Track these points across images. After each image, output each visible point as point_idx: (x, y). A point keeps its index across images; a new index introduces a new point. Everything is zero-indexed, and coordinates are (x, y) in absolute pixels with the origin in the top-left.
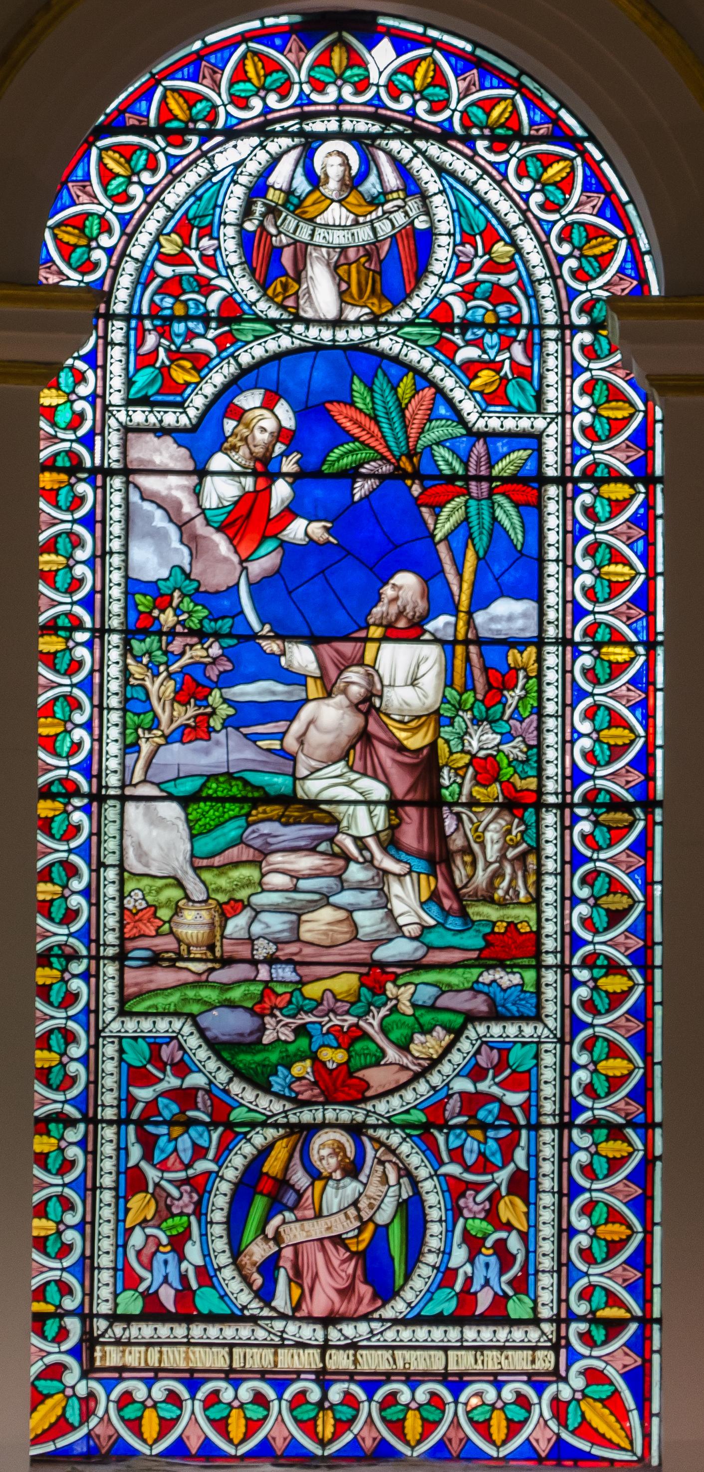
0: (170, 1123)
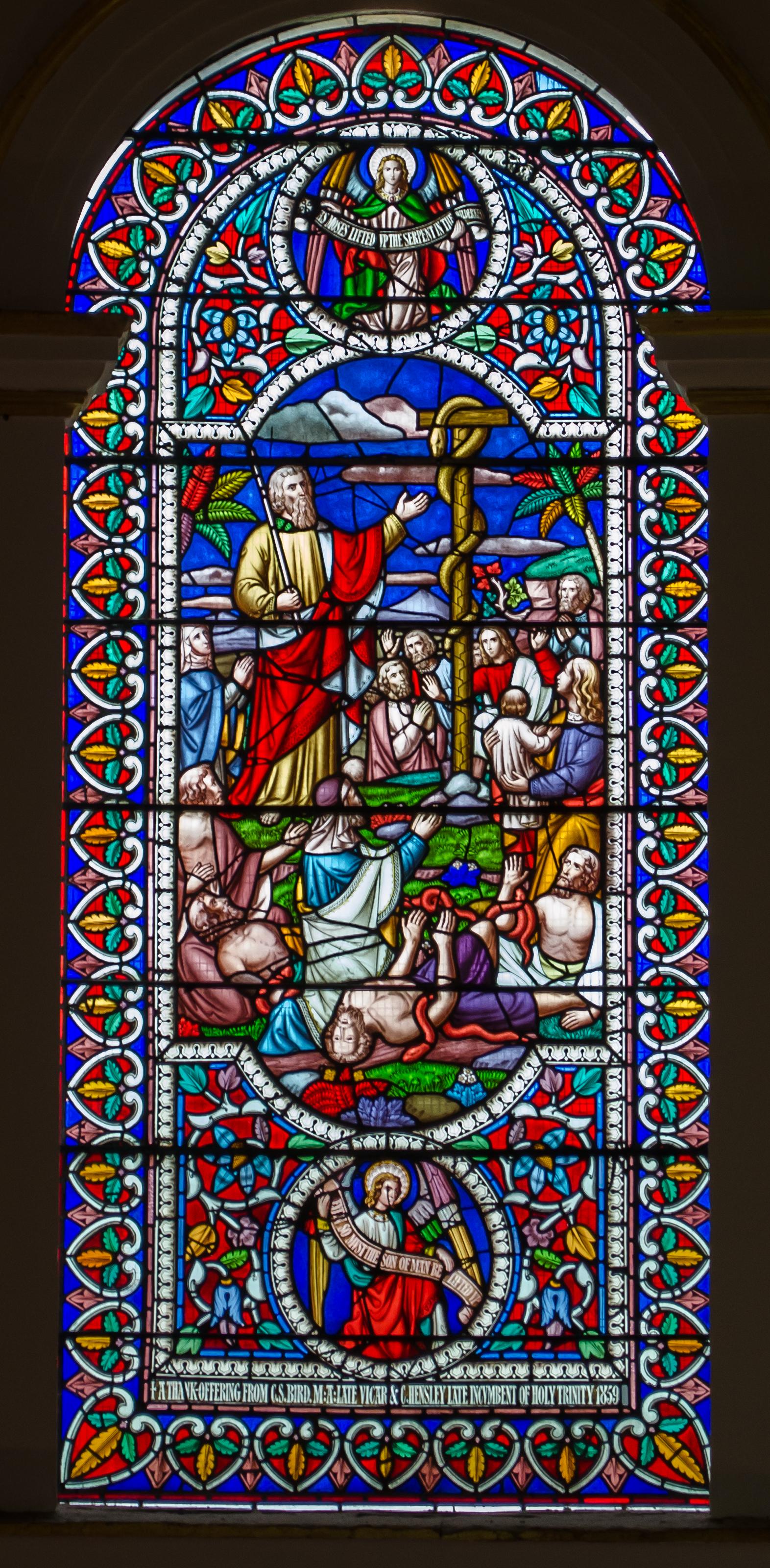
0: (231, 1151)
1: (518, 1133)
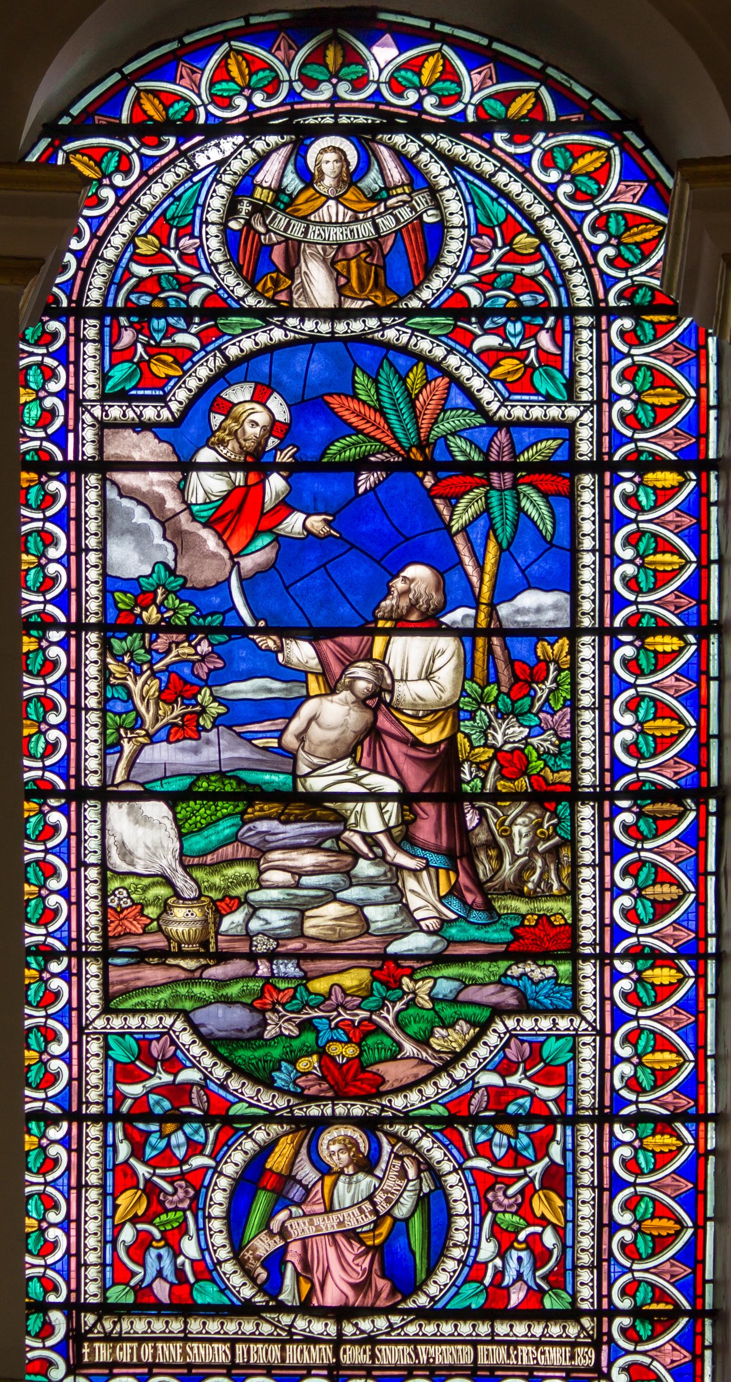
0: (162, 1119)
1: (480, 1102)
